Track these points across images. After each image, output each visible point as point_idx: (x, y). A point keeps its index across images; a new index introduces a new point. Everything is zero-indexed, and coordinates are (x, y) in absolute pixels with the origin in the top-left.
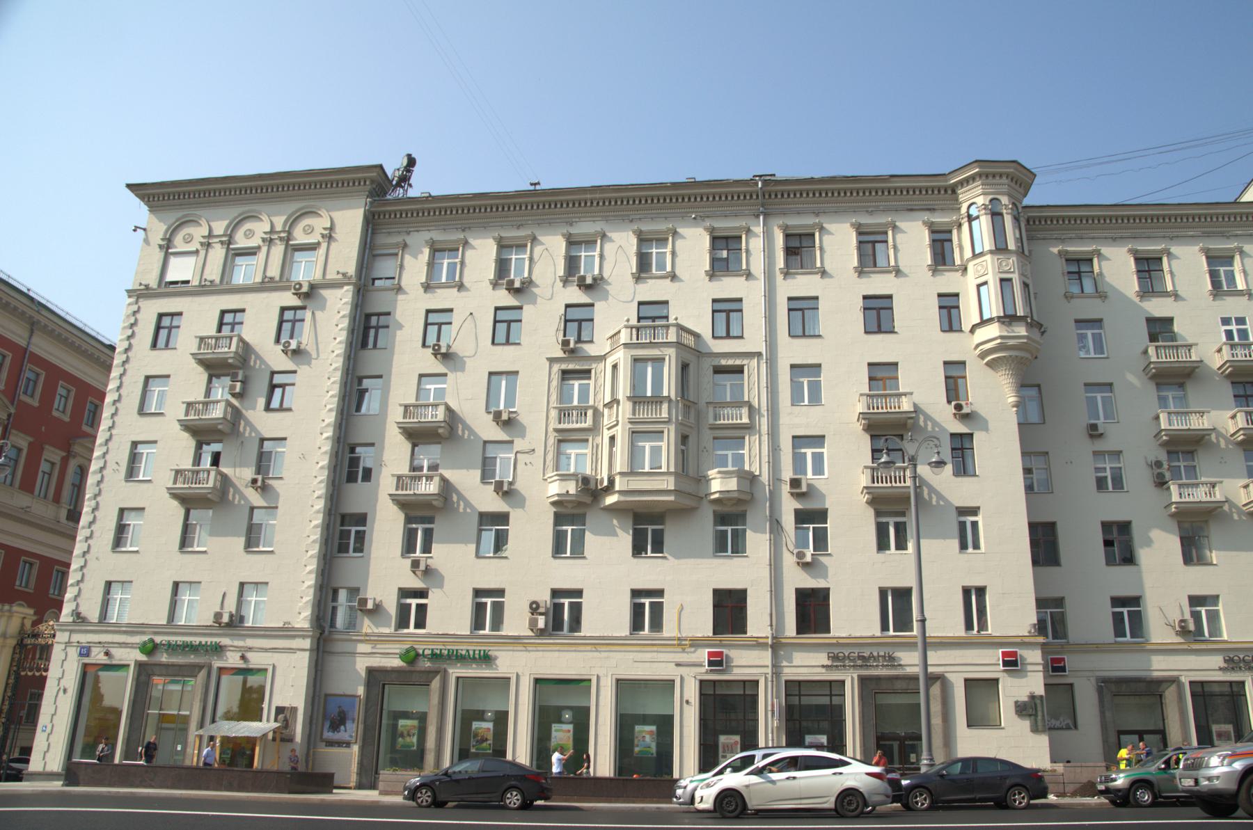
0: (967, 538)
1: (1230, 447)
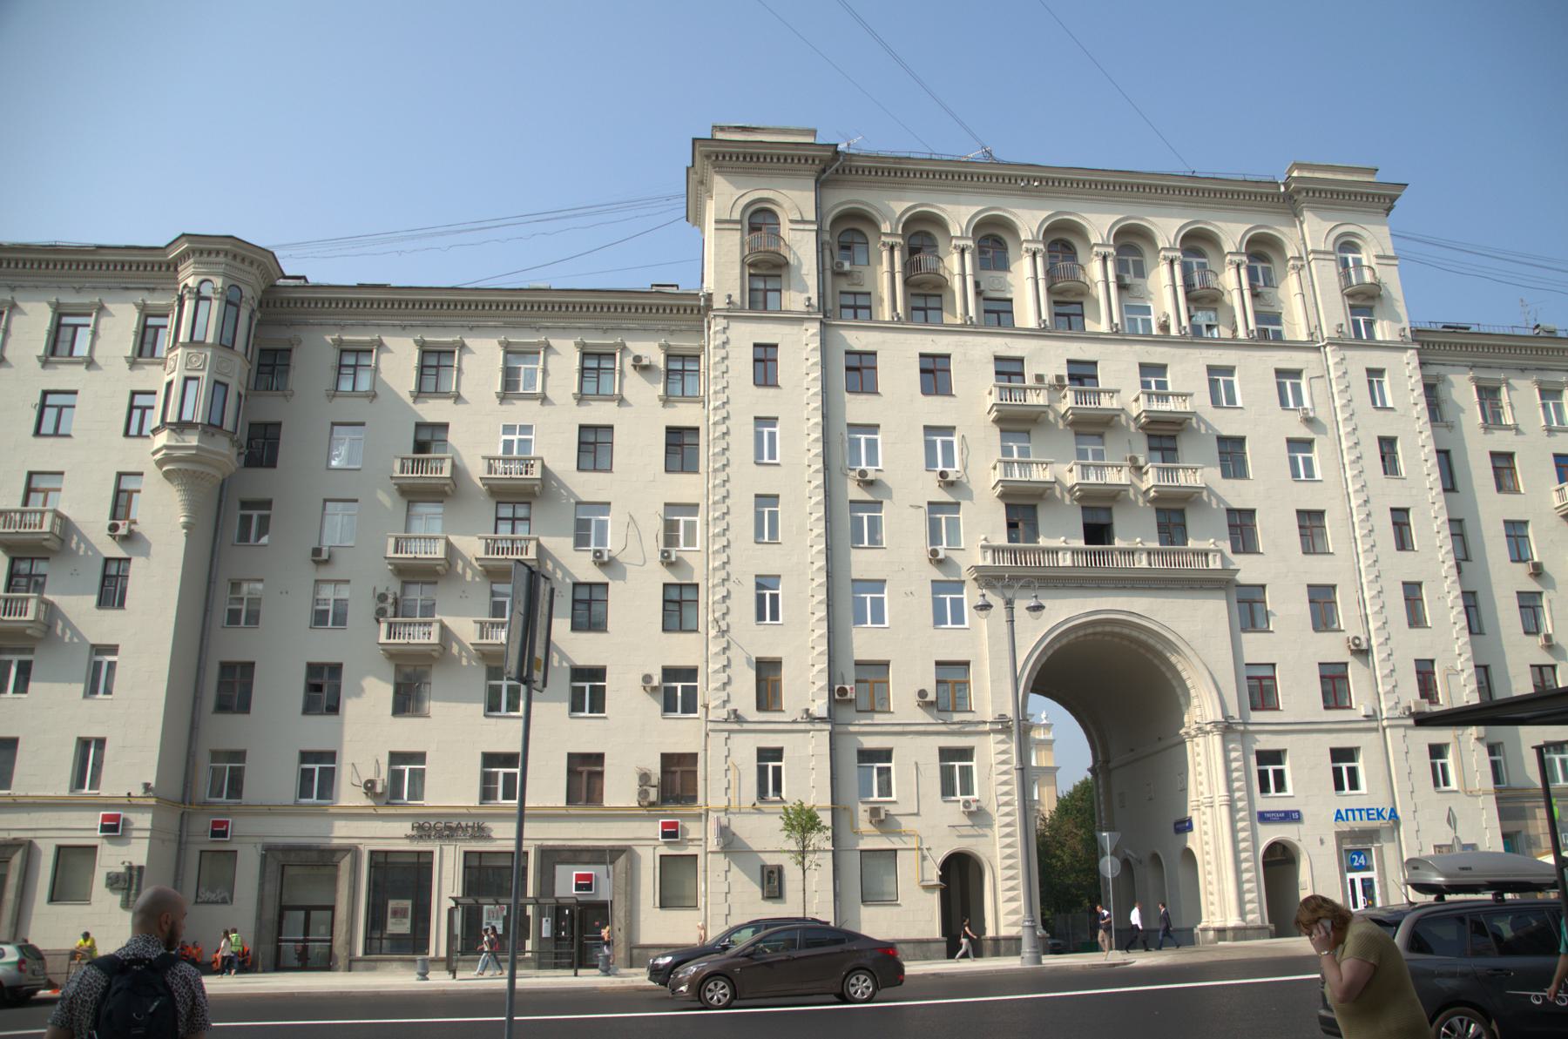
0: (98, 679)
1: (477, 579)
